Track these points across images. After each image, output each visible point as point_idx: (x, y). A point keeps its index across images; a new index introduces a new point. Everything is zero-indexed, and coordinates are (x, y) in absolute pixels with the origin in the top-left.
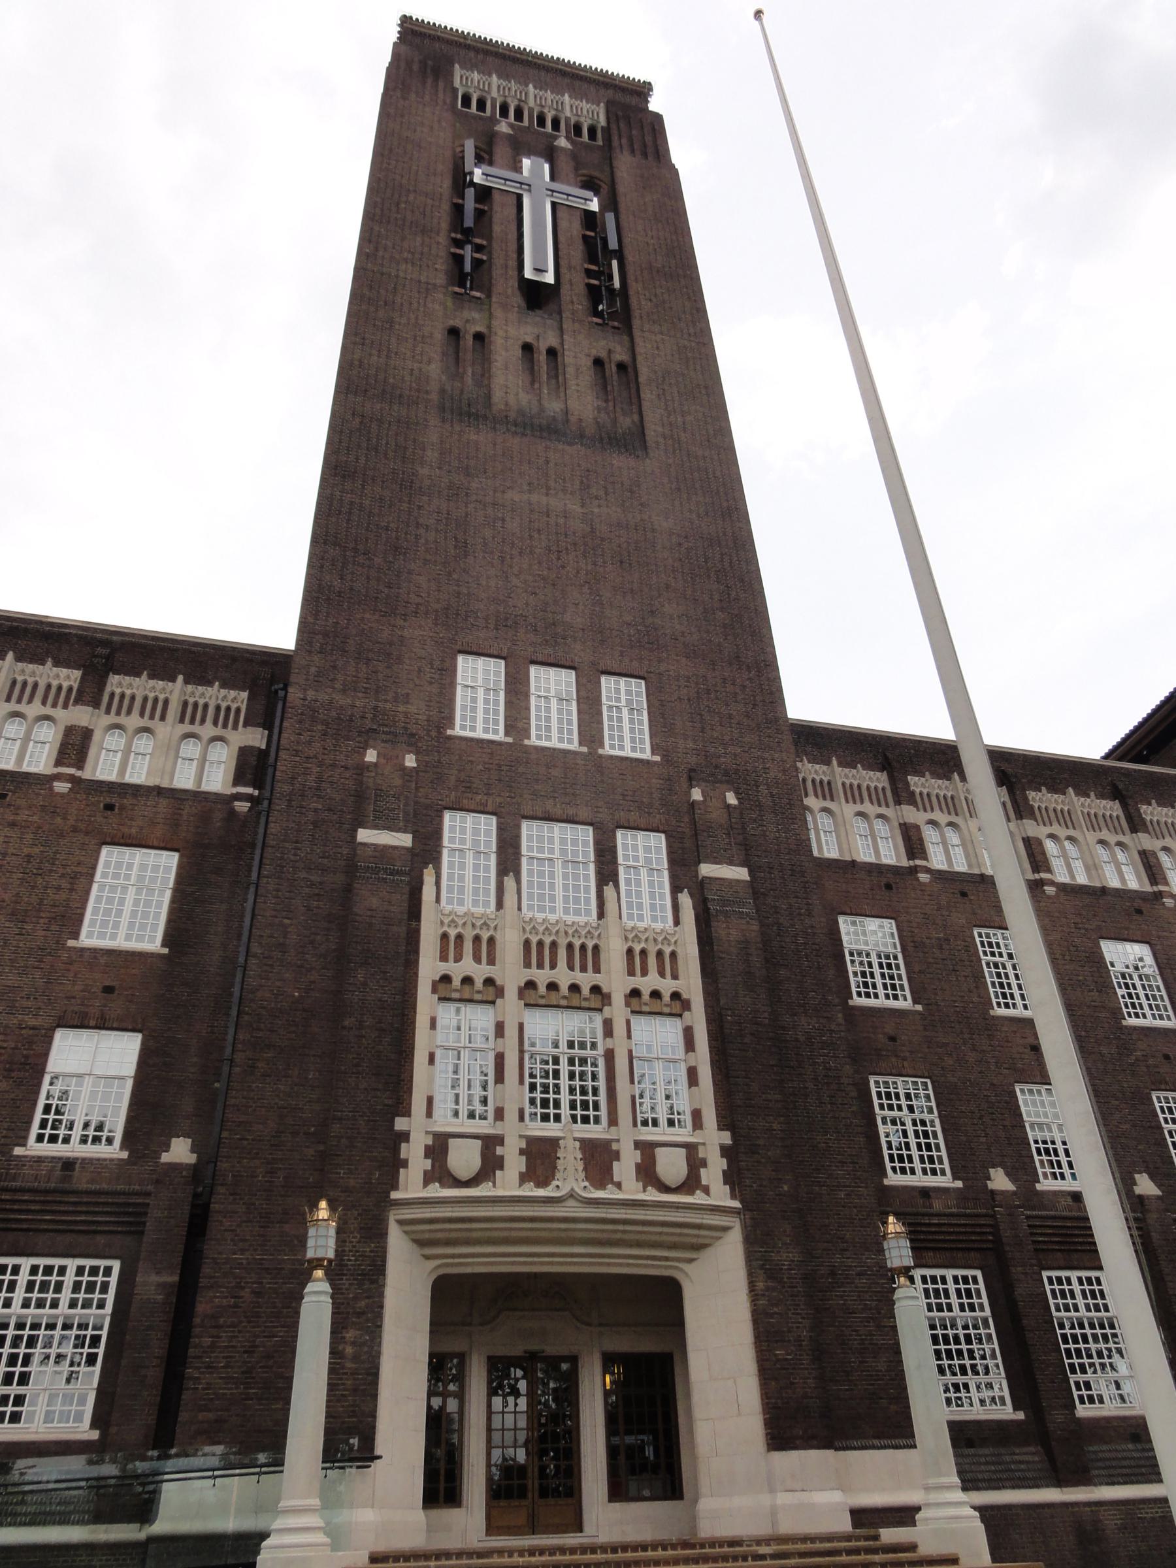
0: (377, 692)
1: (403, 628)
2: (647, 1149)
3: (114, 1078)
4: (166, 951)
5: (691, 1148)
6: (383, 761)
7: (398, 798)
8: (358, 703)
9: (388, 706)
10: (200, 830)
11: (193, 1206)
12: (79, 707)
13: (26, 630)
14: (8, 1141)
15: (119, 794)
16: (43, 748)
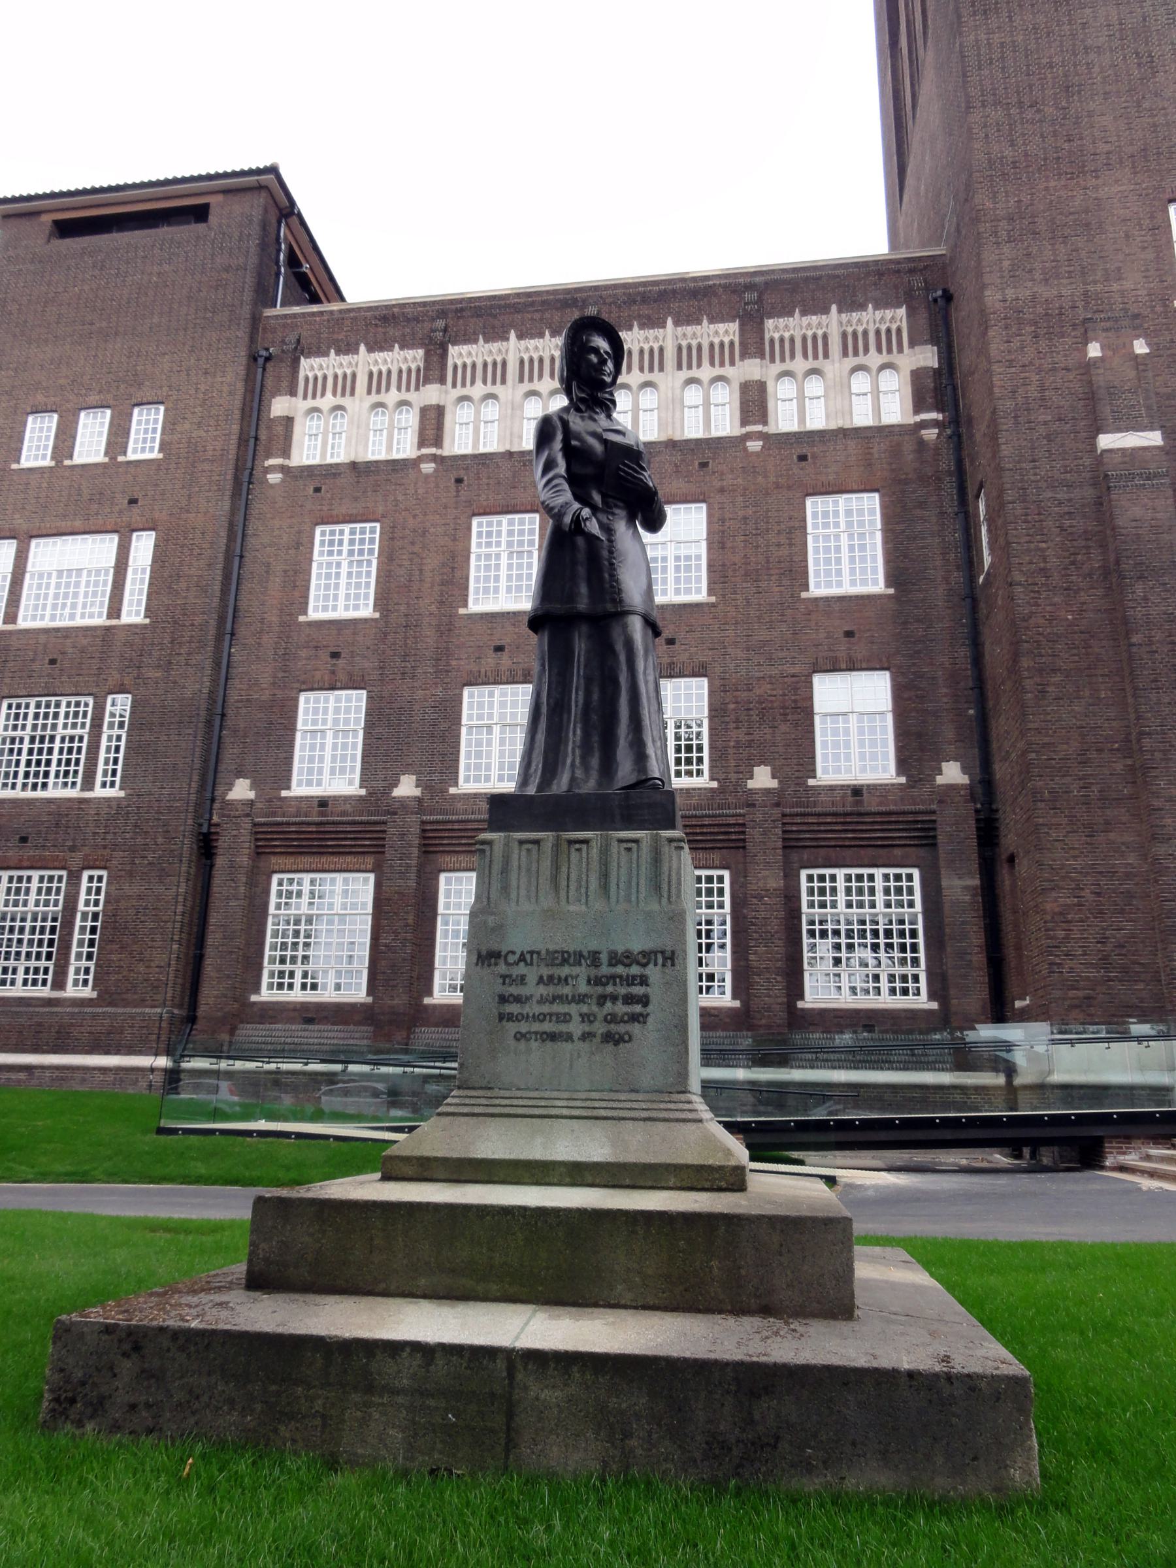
0: (1083, 274)
1: (1096, 188)
3: (838, 715)
4: (891, 591)
6: (1110, 353)
8: (1063, 292)
9: (1099, 287)
10: (894, 466)
11: (978, 821)
12: (747, 362)
13: (674, 291)
14: (800, 774)
15: (808, 443)
16: (467, 429)
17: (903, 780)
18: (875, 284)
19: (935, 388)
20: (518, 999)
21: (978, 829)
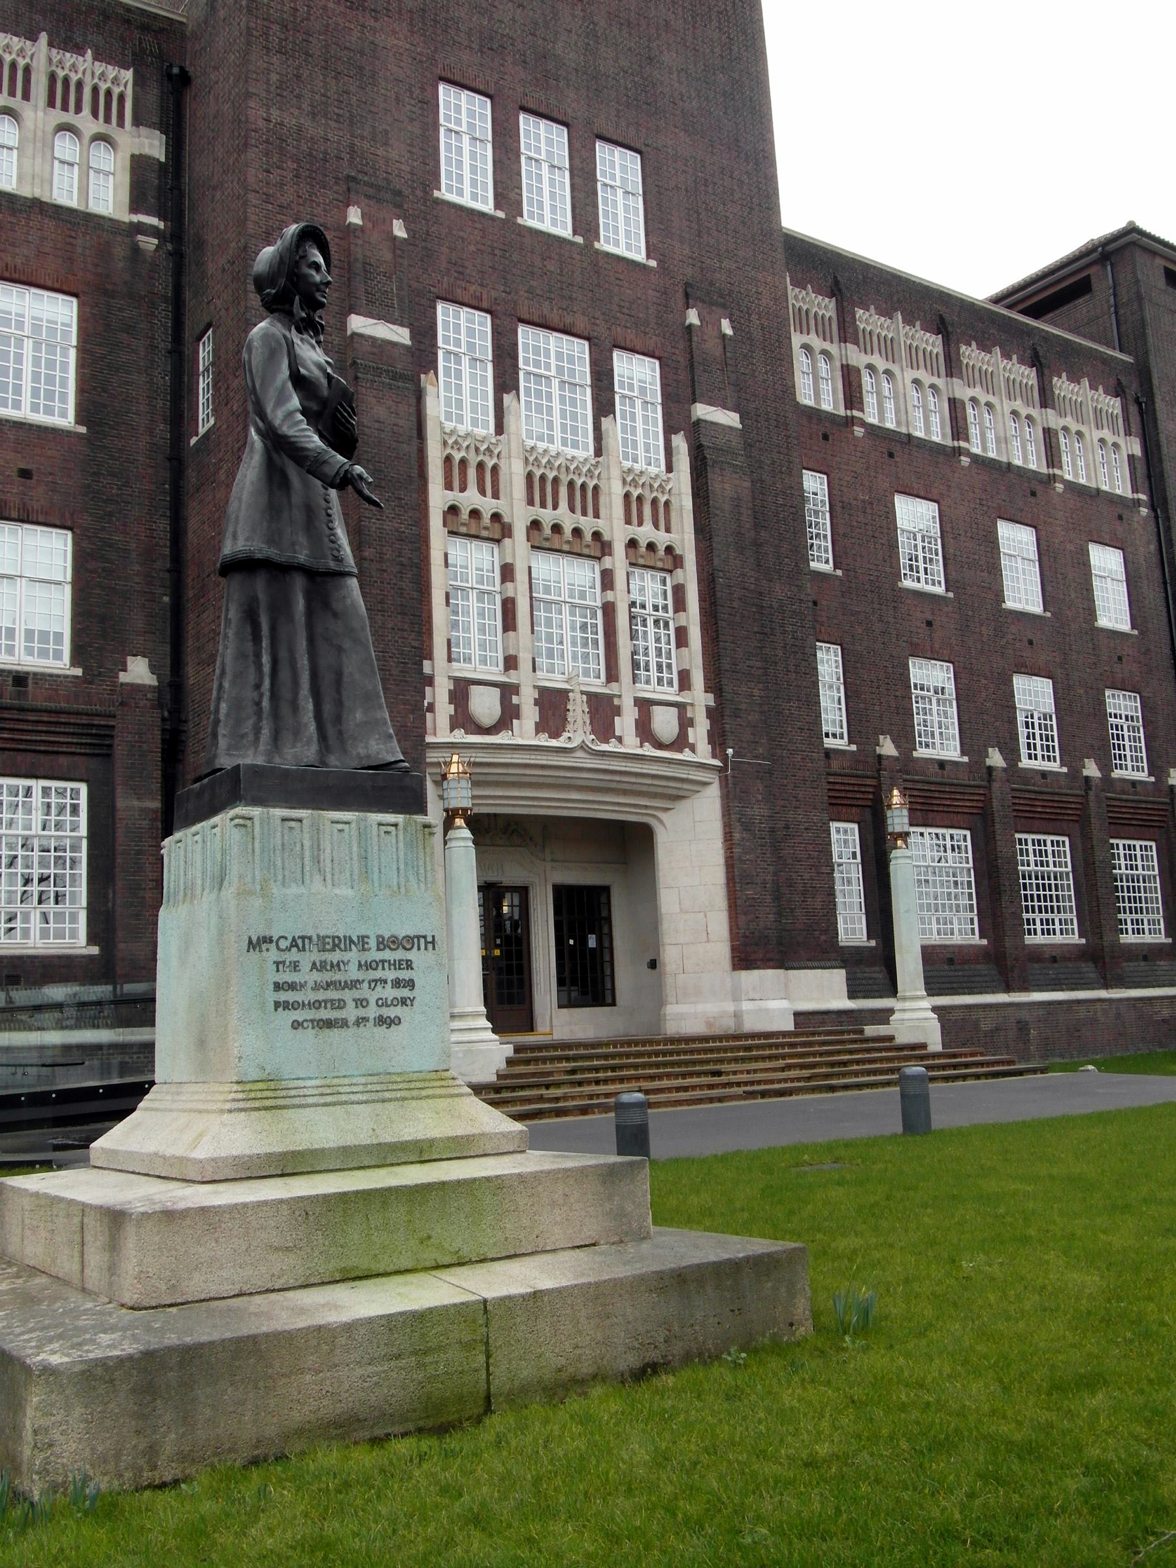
2: (644, 706)
5: (681, 707)
6: (370, 225)
7: (390, 278)
8: (330, 136)
10: (99, 270)
11: (163, 730)
17: (78, 672)
18: (98, 26)
19: (159, 188)
20: (292, 987)
21: (163, 741)
